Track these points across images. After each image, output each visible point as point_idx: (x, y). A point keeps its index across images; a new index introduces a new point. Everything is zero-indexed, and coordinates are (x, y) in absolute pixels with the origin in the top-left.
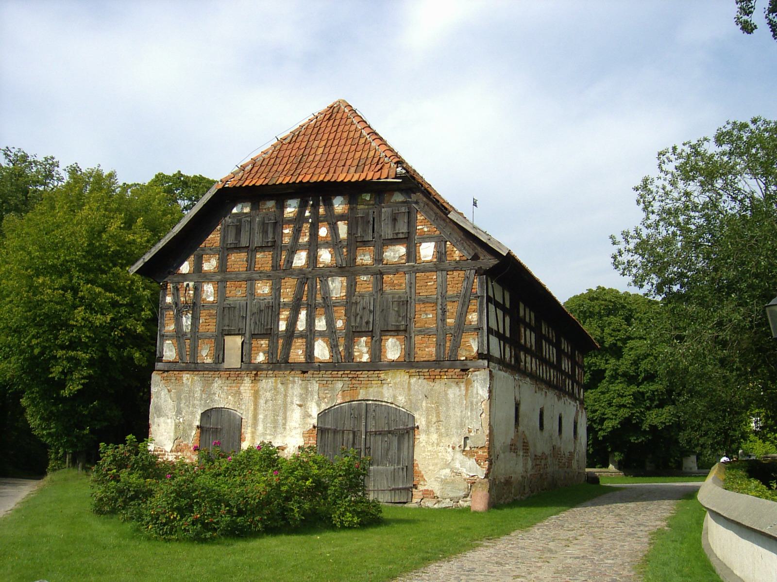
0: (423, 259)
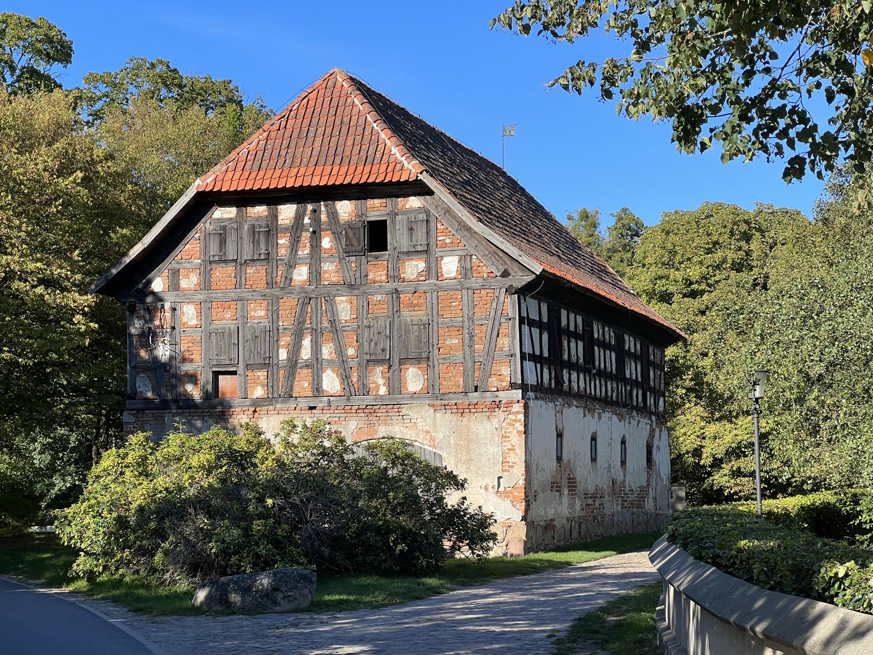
0: (446, 276)
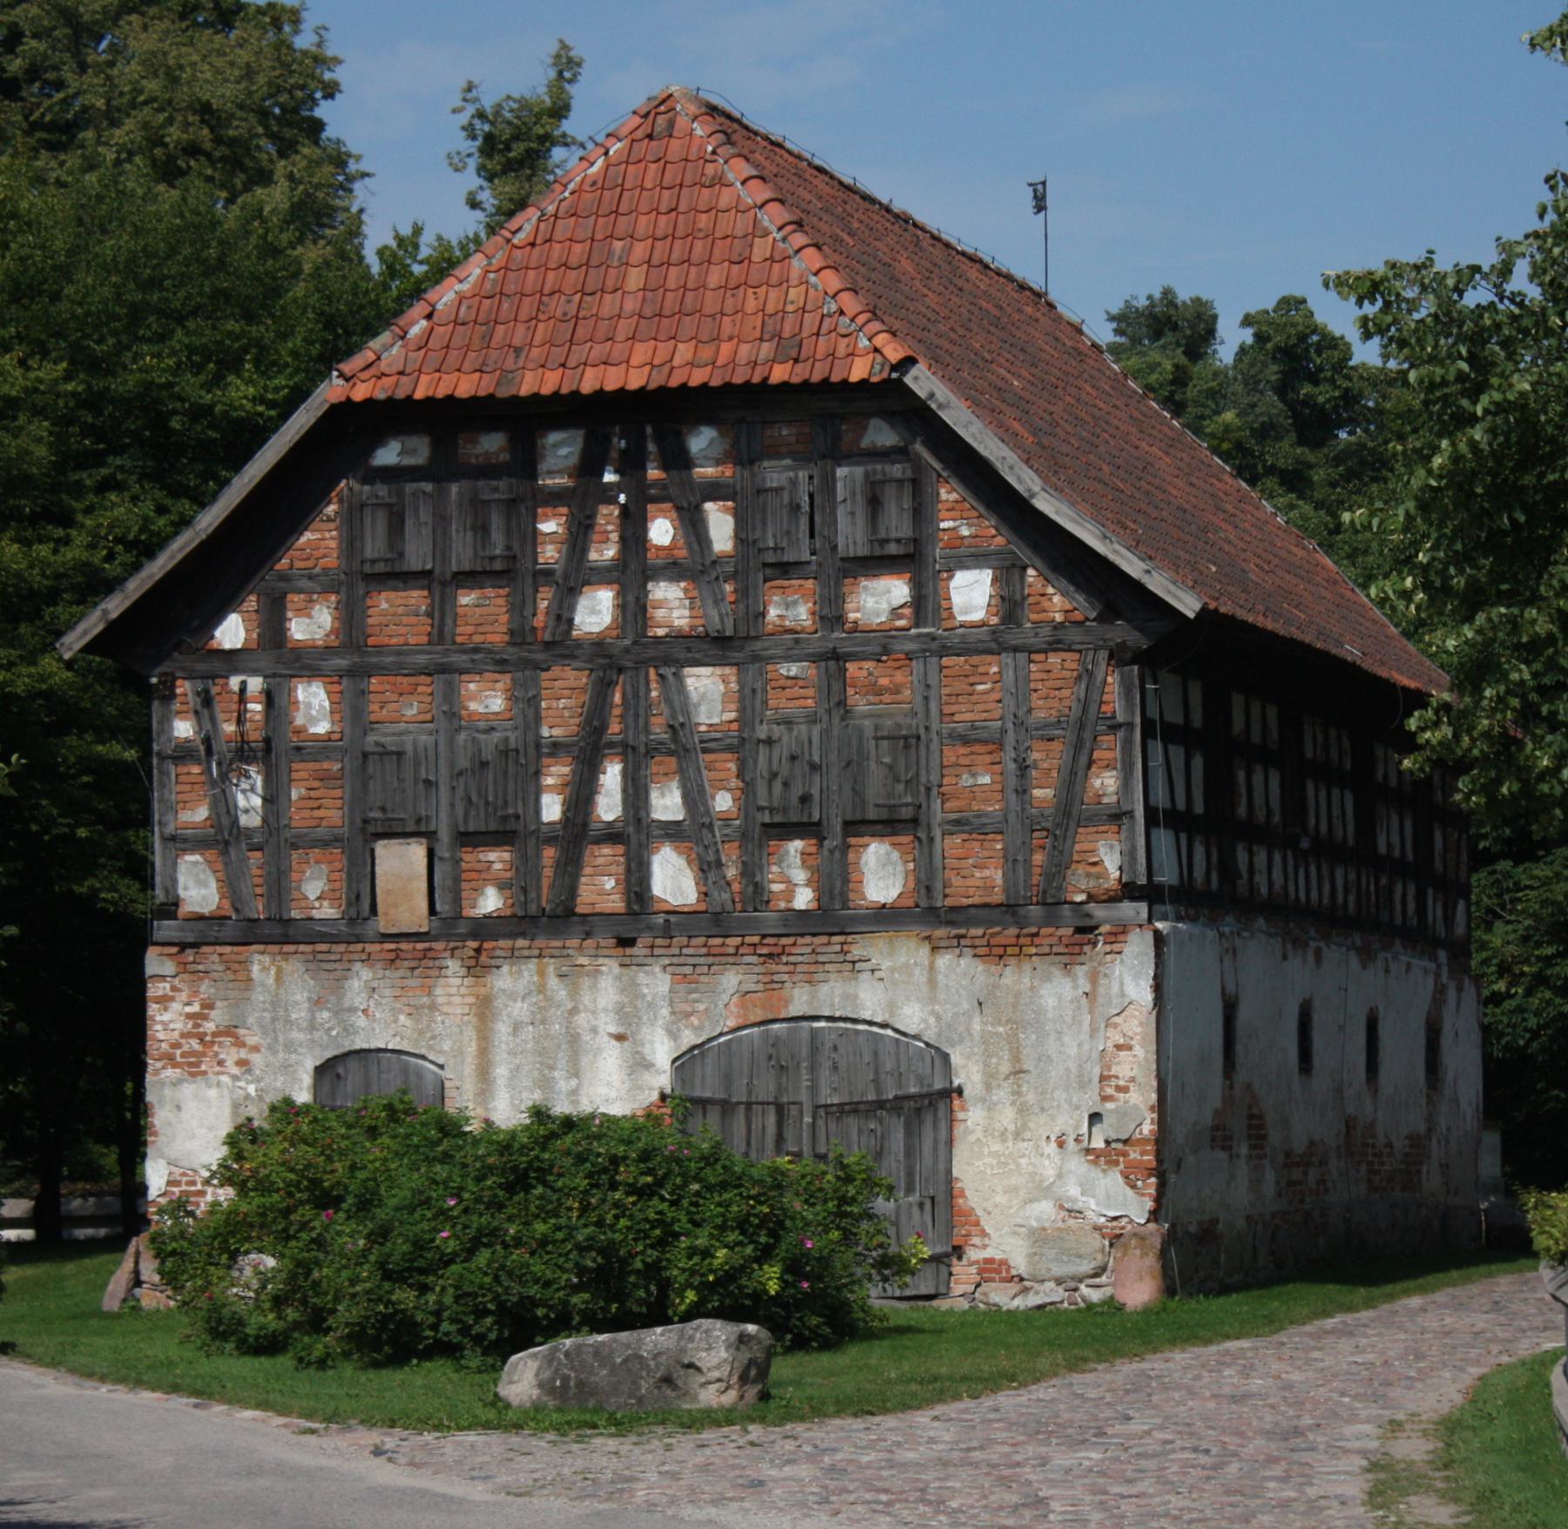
0: (961, 618)
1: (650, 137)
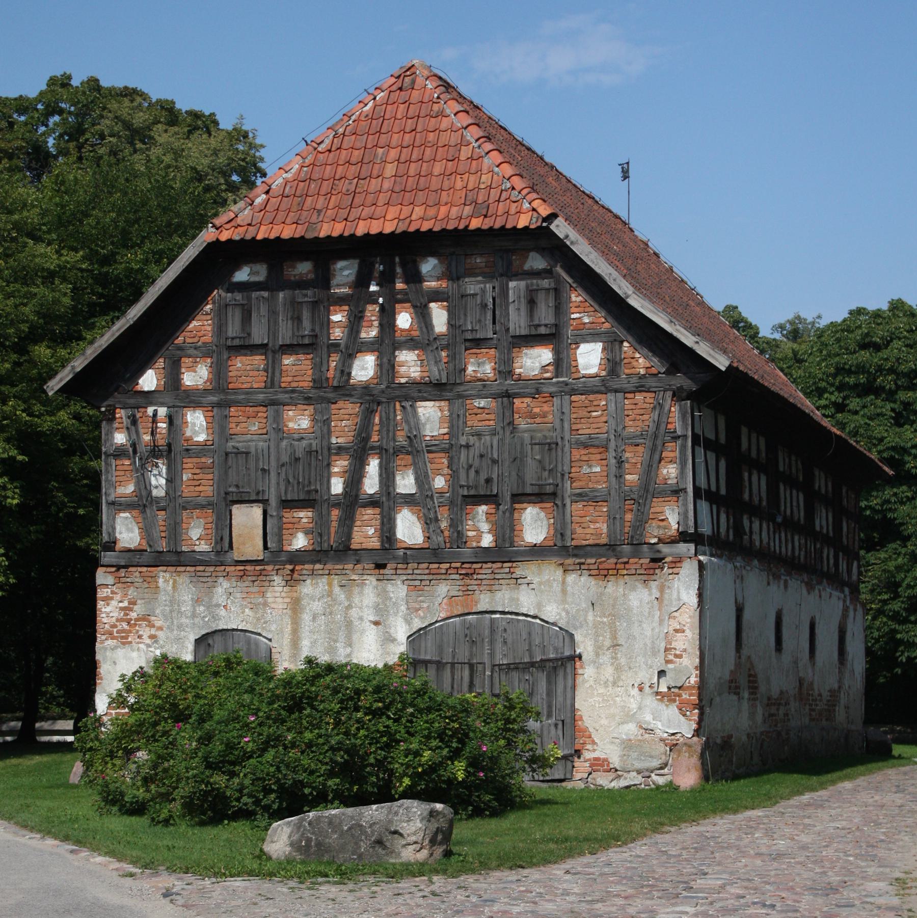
1: (400, 89)
